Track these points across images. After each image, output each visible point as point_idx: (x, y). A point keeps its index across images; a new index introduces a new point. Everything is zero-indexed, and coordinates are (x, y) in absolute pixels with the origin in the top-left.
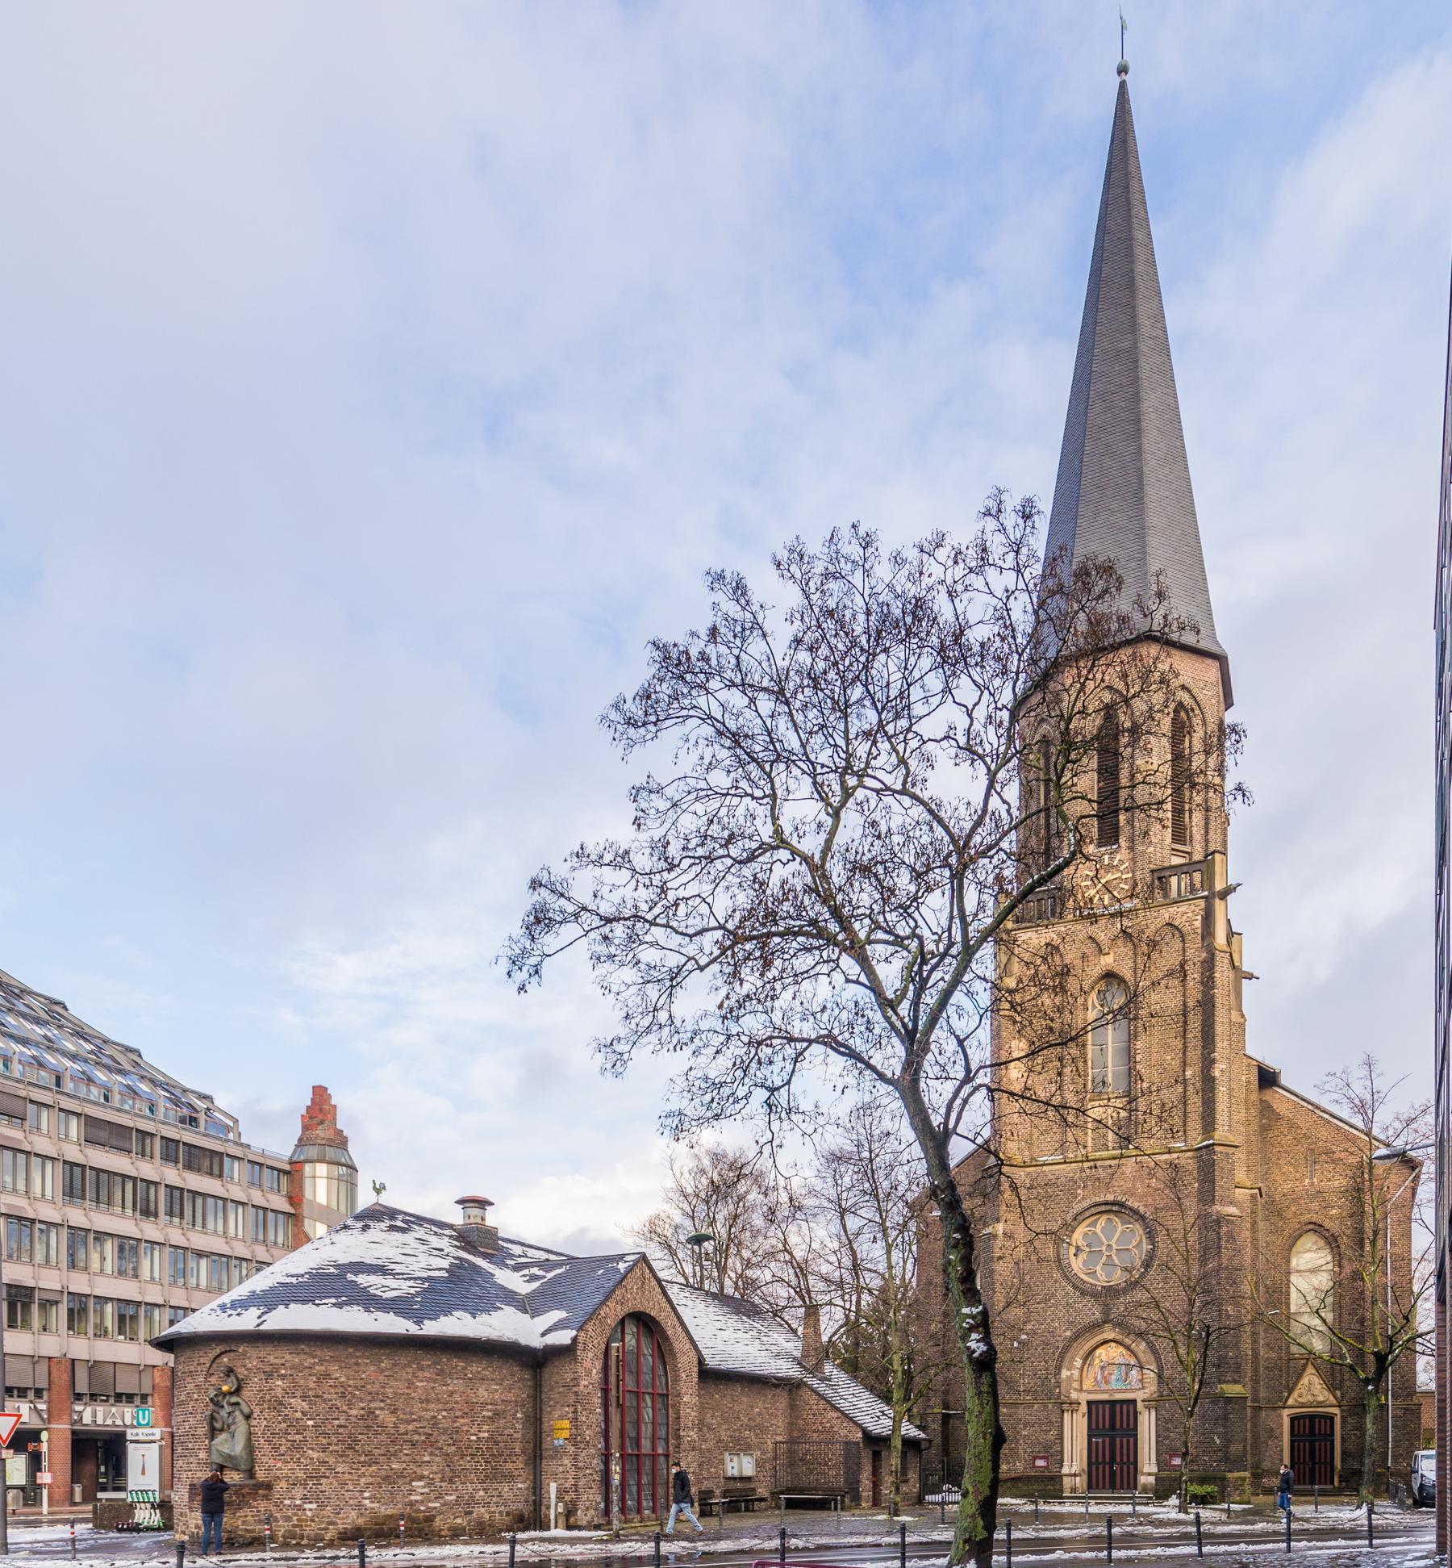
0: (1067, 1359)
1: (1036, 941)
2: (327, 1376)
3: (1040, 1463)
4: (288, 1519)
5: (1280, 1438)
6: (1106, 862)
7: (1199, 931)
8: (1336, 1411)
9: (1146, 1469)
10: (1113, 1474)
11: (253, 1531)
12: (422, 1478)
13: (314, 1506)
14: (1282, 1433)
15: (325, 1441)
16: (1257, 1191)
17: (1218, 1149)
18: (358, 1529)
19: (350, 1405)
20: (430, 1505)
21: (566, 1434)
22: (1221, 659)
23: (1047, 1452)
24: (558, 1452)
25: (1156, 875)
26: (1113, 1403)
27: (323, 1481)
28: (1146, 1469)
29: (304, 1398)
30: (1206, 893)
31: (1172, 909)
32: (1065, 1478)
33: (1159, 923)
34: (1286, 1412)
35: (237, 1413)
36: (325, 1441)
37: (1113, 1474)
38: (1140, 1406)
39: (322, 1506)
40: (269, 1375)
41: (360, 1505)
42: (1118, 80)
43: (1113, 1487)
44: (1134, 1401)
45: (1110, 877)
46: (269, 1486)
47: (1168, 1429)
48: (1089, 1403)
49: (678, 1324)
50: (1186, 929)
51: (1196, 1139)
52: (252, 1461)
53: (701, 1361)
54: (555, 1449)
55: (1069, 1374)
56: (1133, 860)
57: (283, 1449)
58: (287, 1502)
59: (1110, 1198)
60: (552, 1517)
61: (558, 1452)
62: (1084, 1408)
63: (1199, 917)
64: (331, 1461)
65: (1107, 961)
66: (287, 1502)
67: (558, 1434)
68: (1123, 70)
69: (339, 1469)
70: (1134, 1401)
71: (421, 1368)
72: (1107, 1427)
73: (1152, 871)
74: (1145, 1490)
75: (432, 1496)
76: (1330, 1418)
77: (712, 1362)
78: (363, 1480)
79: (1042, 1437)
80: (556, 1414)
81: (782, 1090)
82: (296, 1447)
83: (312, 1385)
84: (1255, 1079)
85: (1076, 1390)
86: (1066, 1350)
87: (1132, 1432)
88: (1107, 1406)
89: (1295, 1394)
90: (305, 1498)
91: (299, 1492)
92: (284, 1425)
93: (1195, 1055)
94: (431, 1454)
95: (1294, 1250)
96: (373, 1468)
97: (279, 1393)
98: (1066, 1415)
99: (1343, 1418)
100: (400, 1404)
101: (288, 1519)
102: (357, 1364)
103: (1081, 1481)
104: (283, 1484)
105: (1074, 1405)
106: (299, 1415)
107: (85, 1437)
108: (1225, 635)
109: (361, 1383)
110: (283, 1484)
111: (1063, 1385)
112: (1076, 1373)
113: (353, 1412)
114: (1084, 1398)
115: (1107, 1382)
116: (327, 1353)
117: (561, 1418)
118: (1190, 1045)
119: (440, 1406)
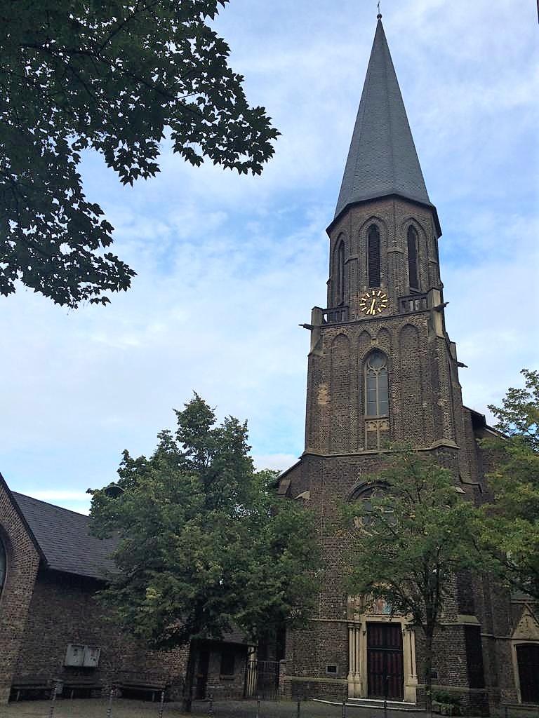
5: (509, 662)
14: (511, 658)
16: (477, 486)
20: (459, 658)
22: (433, 210)
25: (401, 300)
34: (514, 643)
38: (403, 627)
48: (368, 624)
49: (22, 529)
53: (43, 561)
62: (364, 628)
65: (374, 344)
68: (380, 16)
73: (399, 299)
77: (54, 564)
84: (469, 420)
89: (518, 630)
105: (356, 626)
108: (434, 200)
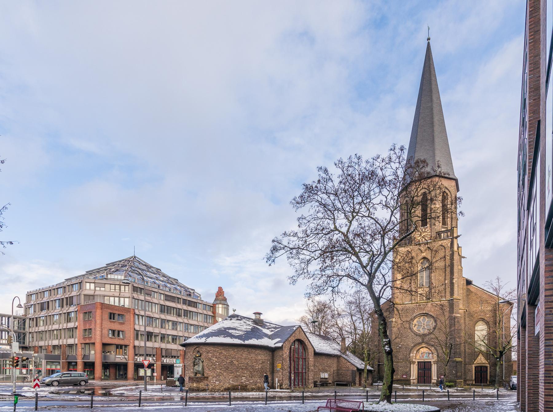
2: (222, 353)
3: (404, 376)
4: (212, 385)
6: (424, 230)
7: (450, 247)
9: (434, 378)
10: (424, 379)
11: (204, 388)
12: (244, 376)
13: (218, 382)
15: (221, 368)
17: (454, 300)
18: (229, 388)
19: (227, 360)
21: (280, 367)
24: (278, 371)
26: (425, 362)
27: (220, 377)
28: (434, 378)
29: (216, 358)
30: (451, 237)
31: (442, 242)
32: (411, 380)
33: (438, 245)
34: (474, 366)
35: (200, 361)
36: (221, 368)
37: (424, 379)
38: (432, 363)
39: (220, 382)
40: (208, 353)
41: (229, 382)
42: (427, 42)
43: (425, 383)
44: (431, 362)
45: (424, 234)
46: (207, 378)
47: (440, 369)
50: (446, 246)
51: (448, 297)
52: (204, 372)
54: (277, 371)
56: (431, 230)
57: (211, 369)
58: (212, 381)
59: (424, 312)
60: (277, 386)
61: (278, 371)
62: (417, 363)
63: (450, 243)
64: (222, 372)
65: (424, 255)
66: (212, 381)
67: (278, 367)
69: (224, 374)
70: (431, 362)
71: (244, 352)
72: (423, 368)
74: (433, 383)
75: (247, 381)
76: (487, 367)
78: (230, 377)
79: (405, 370)
80: (278, 363)
82: (214, 369)
83: (218, 355)
87: (430, 369)
88: (423, 363)
90: (216, 381)
91: (215, 379)
92: (211, 364)
93: (448, 277)
94: (247, 371)
96: (233, 374)
97: (210, 356)
98: (412, 365)
99: (490, 367)
100: (239, 360)
101: (212, 385)
102: (229, 350)
104: (211, 377)
106: (215, 362)
109: (230, 355)
110: (211, 377)
111: (411, 358)
112: (415, 355)
113: (228, 361)
114: (417, 361)
115: (423, 357)
116: (221, 348)
117: (279, 363)
118: (447, 275)
119: (249, 360)
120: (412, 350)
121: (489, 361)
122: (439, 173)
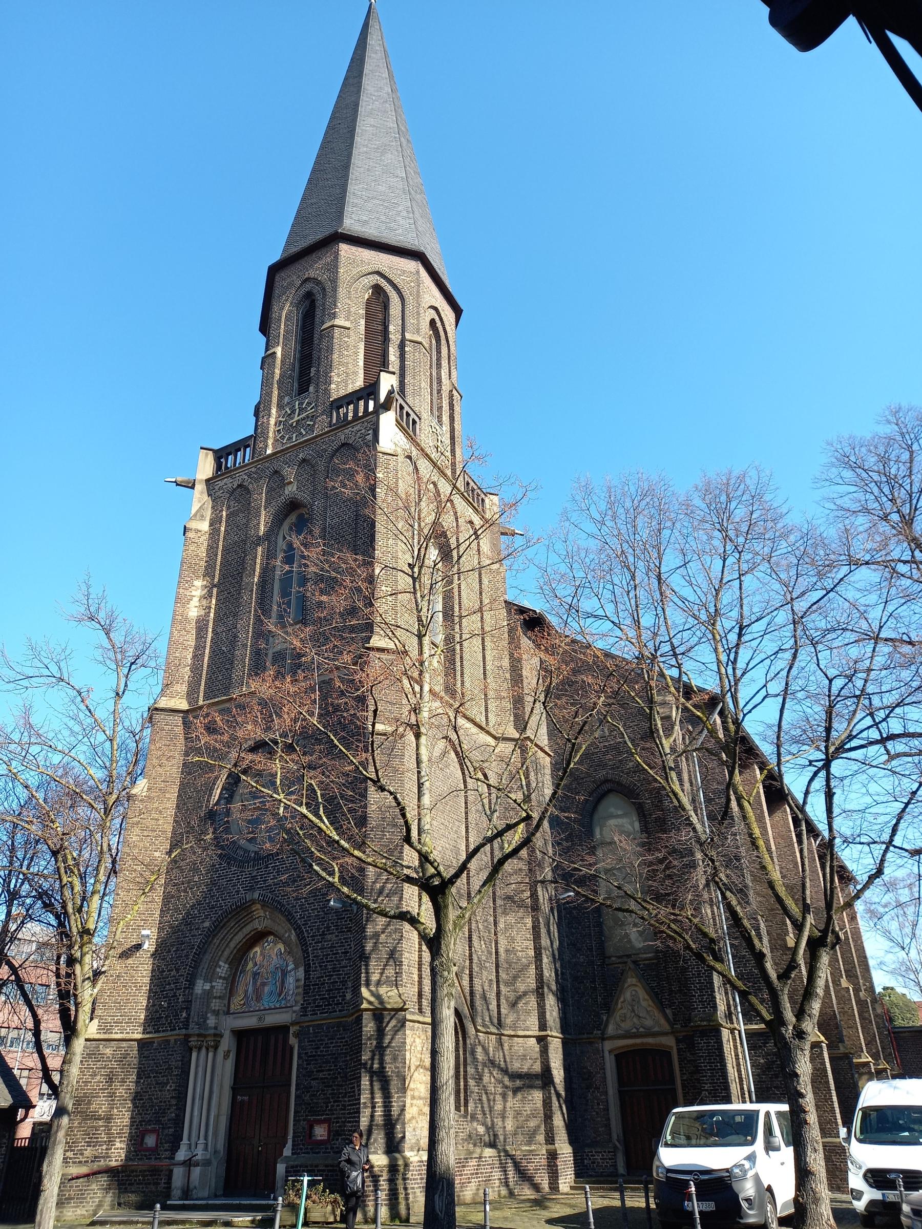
0: (204, 965)
1: (230, 485)
8: (669, 1041)
23: (158, 1122)
34: (608, 1045)
48: (240, 1035)
55: (207, 987)
62: (227, 1043)
76: (664, 1054)
81: (480, 841)
85: (216, 1013)
86: (203, 949)
95: (596, 817)
99: (679, 1050)
103: (202, 1174)
107: (884, 1136)
111: (195, 1007)
115: (259, 998)
120: (208, 957)
121: (668, 1011)
122: (591, 540)
